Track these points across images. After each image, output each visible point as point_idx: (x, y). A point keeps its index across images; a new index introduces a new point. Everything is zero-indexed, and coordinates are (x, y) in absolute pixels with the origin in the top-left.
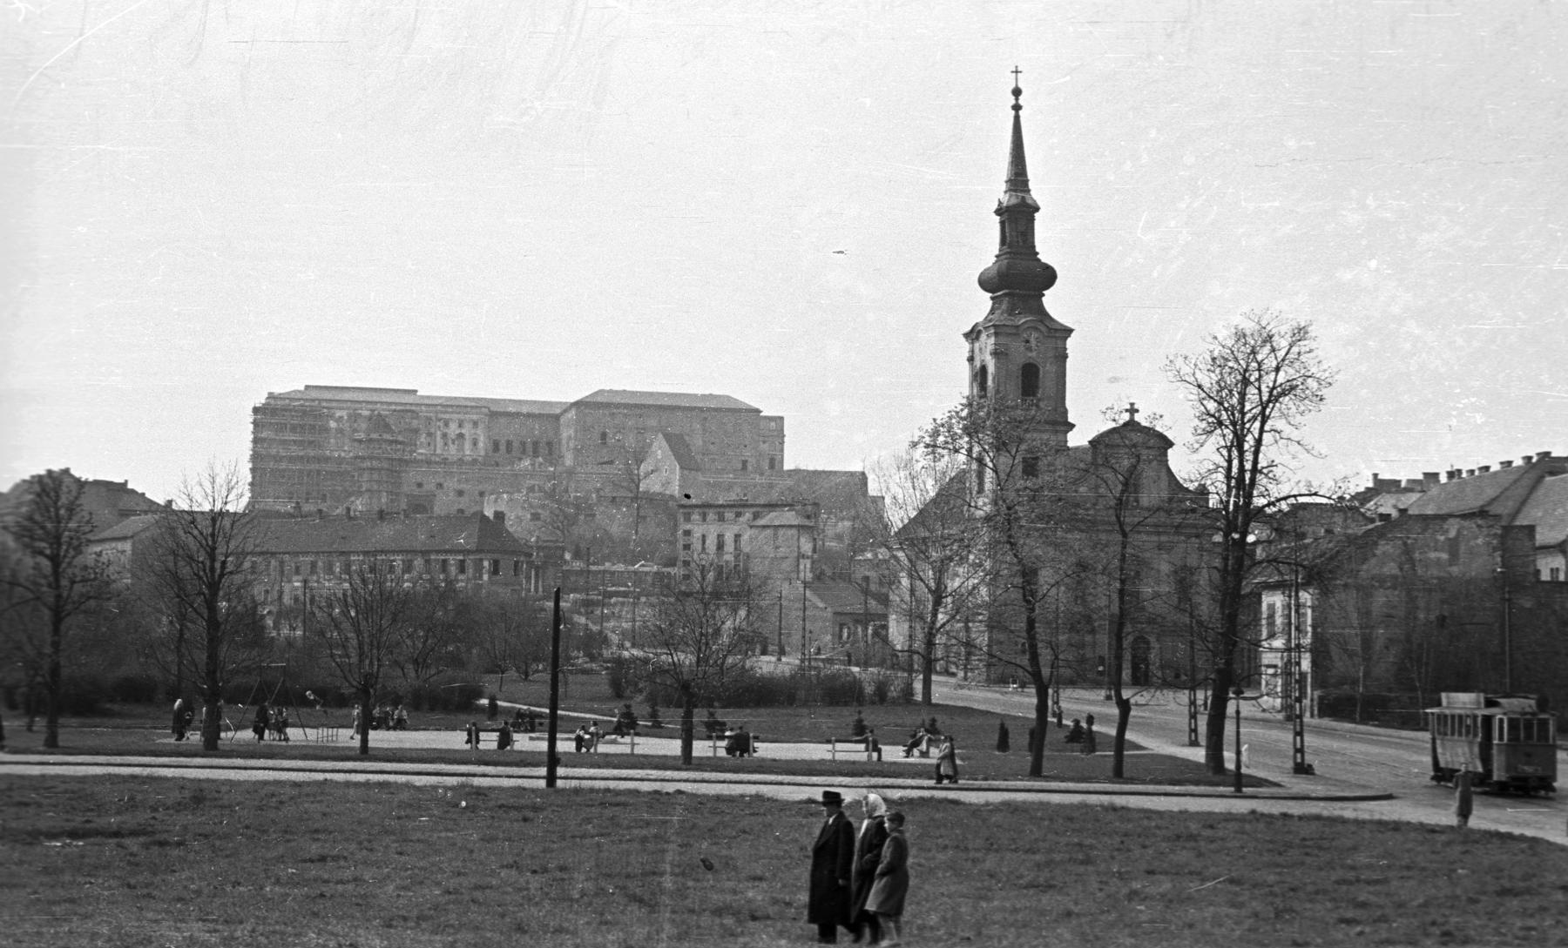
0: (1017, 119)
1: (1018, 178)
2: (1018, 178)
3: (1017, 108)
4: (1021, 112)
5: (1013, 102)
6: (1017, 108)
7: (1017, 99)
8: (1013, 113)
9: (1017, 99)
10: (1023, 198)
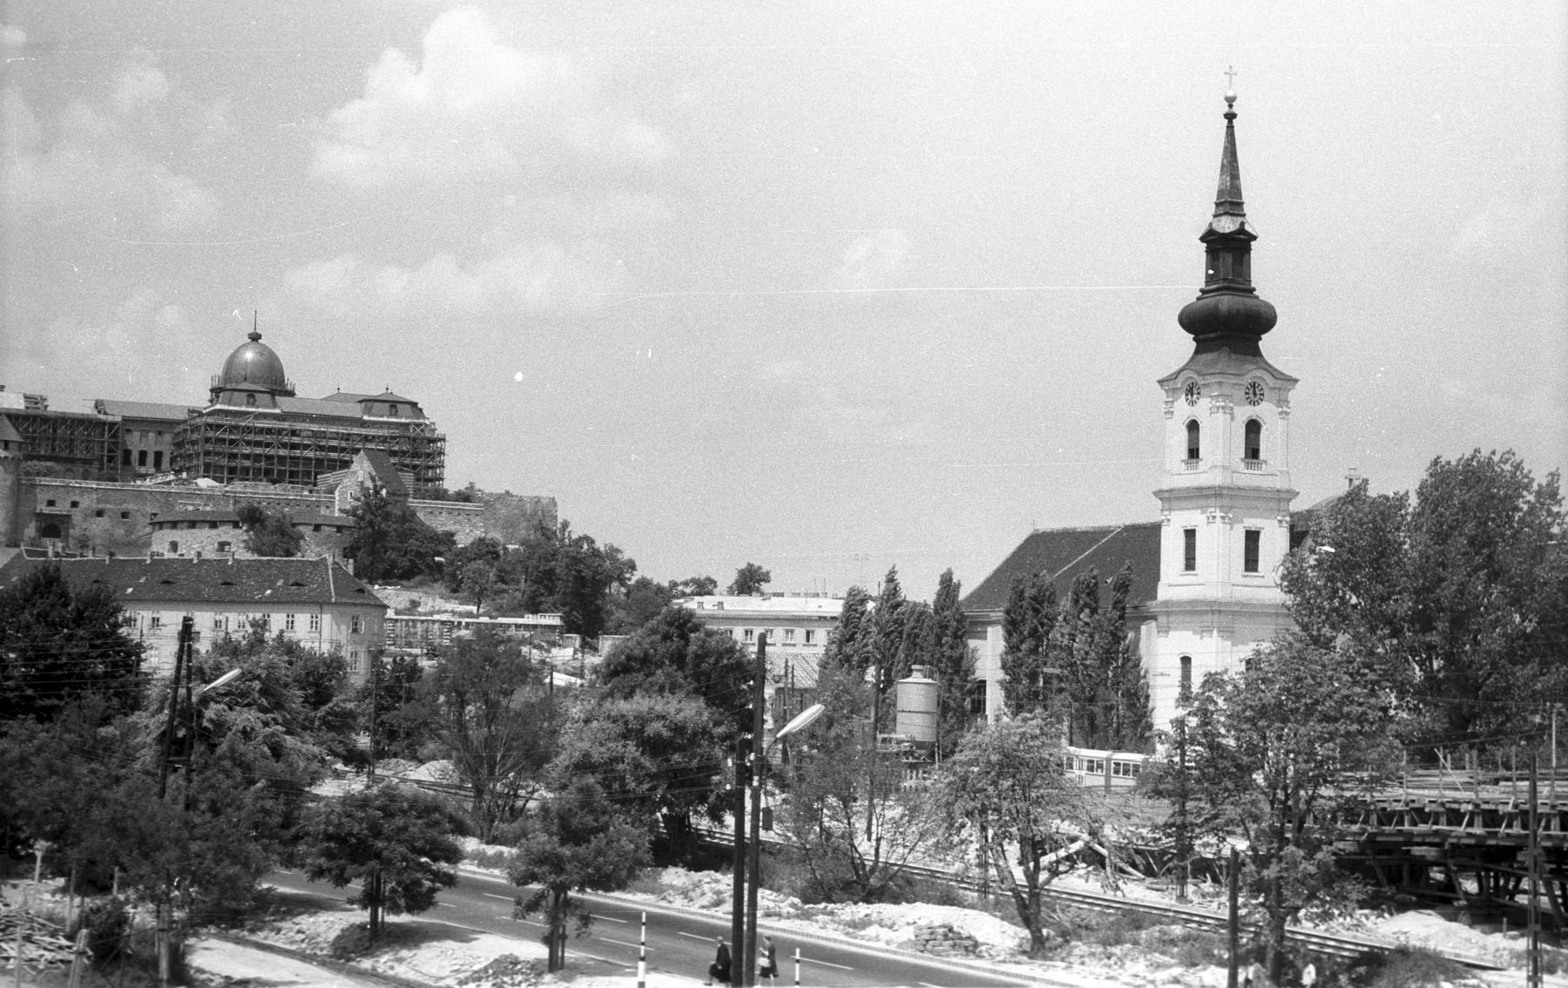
0: (1230, 128)
1: (1230, 202)
2: (1230, 202)
3: (1230, 117)
4: (1235, 121)
5: (1226, 109)
6: (1230, 117)
7: (1231, 106)
9: (1231, 106)
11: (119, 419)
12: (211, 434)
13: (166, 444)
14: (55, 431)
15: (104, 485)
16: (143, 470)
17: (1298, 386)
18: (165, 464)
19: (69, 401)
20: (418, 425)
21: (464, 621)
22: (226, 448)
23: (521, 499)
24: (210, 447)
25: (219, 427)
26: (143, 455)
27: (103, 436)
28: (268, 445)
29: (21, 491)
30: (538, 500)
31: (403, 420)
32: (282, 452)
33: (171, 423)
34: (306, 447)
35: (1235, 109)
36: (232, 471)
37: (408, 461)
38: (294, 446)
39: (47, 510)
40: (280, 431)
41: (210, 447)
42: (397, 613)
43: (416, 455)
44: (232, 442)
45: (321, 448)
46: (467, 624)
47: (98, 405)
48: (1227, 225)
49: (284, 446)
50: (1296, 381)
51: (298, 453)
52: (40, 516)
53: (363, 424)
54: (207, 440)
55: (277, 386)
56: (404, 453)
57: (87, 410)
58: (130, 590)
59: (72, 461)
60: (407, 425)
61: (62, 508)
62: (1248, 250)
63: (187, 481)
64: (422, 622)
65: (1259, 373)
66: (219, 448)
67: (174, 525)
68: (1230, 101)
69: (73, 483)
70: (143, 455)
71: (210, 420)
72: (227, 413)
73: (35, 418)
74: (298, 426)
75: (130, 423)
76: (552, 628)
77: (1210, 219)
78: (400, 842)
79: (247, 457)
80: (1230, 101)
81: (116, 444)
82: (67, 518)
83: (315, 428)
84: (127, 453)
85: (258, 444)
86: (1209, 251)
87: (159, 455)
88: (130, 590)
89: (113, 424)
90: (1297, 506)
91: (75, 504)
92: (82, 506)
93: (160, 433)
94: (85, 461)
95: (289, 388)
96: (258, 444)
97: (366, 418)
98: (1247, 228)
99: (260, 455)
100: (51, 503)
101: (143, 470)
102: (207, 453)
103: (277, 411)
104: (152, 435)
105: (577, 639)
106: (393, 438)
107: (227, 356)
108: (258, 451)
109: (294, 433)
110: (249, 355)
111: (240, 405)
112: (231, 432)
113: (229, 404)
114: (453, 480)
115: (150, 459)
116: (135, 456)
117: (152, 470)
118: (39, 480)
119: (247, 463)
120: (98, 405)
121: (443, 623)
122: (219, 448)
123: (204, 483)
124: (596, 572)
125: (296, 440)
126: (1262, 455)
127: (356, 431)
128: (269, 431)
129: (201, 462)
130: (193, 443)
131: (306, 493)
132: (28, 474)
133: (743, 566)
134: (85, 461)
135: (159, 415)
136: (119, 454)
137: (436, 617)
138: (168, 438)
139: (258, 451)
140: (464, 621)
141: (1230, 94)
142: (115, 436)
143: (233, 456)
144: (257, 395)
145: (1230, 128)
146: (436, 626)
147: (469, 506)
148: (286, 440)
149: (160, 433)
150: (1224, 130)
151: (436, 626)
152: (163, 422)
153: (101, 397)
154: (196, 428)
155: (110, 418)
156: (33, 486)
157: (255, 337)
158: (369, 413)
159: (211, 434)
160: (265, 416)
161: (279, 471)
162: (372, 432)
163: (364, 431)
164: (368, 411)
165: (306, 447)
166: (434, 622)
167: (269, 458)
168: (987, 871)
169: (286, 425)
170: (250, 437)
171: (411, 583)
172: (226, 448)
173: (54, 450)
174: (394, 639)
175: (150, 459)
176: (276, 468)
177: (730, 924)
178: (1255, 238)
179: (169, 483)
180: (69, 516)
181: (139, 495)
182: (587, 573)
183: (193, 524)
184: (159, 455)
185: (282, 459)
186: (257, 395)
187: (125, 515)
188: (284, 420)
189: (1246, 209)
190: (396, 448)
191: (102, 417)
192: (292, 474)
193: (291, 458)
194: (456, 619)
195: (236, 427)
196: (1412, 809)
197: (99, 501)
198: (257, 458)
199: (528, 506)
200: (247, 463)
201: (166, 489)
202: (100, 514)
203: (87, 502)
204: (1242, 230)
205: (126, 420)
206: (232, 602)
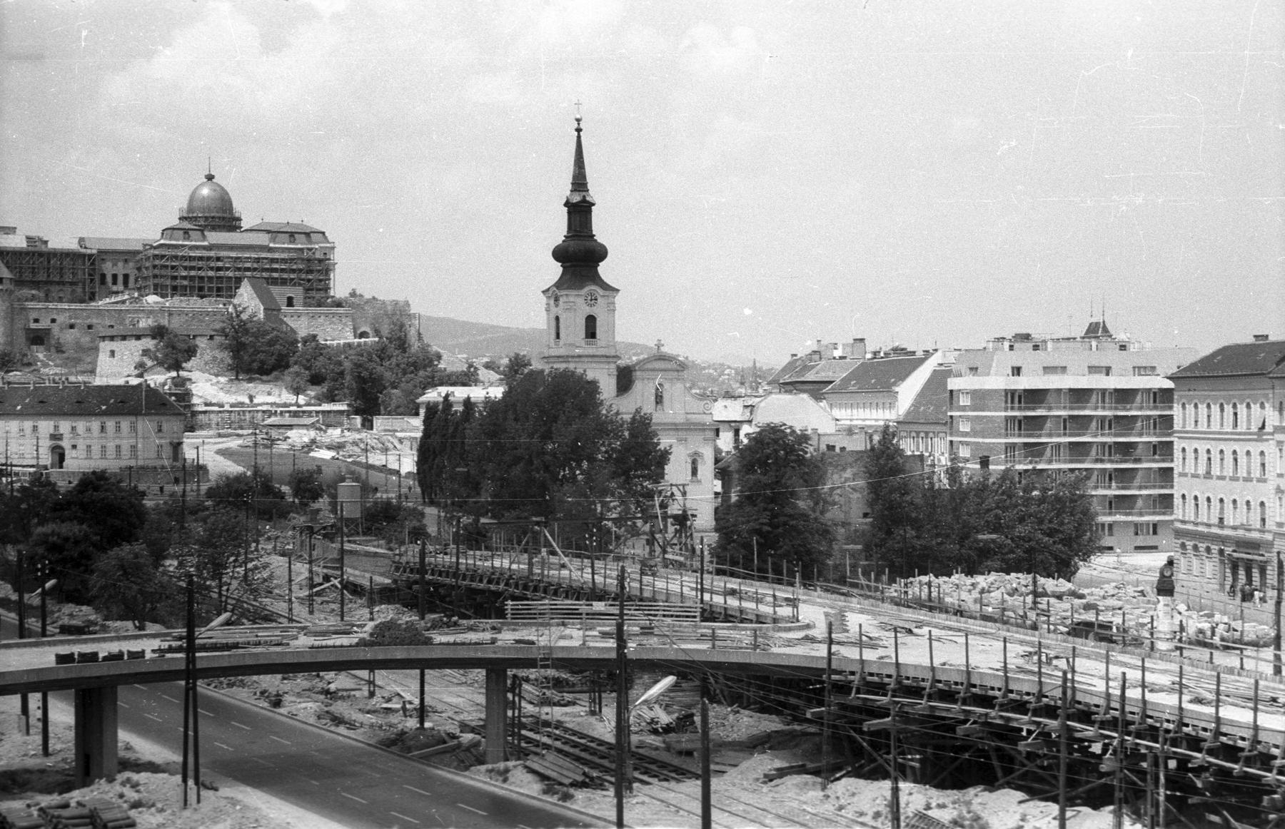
0: (579, 137)
2: (579, 182)
3: (579, 130)
4: (581, 133)
5: (576, 126)
6: (579, 130)
8: (576, 133)
10: (584, 197)
11: (94, 251)
12: (157, 262)
13: (130, 269)
14: (49, 262)
15: (73, 306)
16: (115, 288)
17: (620, 293)
18: (131, 284)
19: (62, 239)
20: (310, 249)
21: (279, 410)
22: (169, 272)
23: (384, 302)
24: (157, 272)
25: (163, 257)
26: (115, 277)
27: (84, 264)
28: (200, 269)
29: (15, 312)
30: (396, 303)
31: (299, 246)
32: (211, 273)
33: (136, 253)
34: (228, 269)
35: (581, 126)
36: (175, 288)
37: (303, 276)
38: (219, 269)
39: (33, 326)
40: (209, 258)
41: (157, 272)
42: (231, 406)
43: (310, 272)
44: (173, 267)
45: (239, 269)
46: (282, 412)
47: (81, 240)
48: (576, 198)
49: (212, 269)
50: (618, 291)
51: (221, 273)
52: (28, 330)
53: (270, 250)
54: (155, 267)
55: (224, 217)
56: (300, 270)
57: (73, 245)
58: (19, 408)
59: (63, 283)
60: (301, 250)
61: (44, 324)
62: (590, 212)
63: (136, 300)
64: (250, 411)
65: (593, 287)
66: (163, 272)
67: (112, 338)
68: (578, 120)
69: (51, 305)
70: (115, 277)
71: (157, 252)
72: (169, 246)
73: (34, 253)
74: (223, 254)
75: (104, 254)
76: (341, 412)
77: (568, 193)
78: (638, 504)
79: (184, 278)
80: (578, 120)
81: (94, 269)
82: (47, 332)
83: (233, 254)
84: (103, 276)
85: (192, 268)
86: (569, 213)
87: (126, 277)
88: (19, 408)
89: (90, 256)
90: (621, 363)
91: (53, 321)
92: (58, 321)
93: (126, 261)
94: (72, 284)
95: (237, 215)
96: (192, 268)
97: (271, 245)
98: (588, 199)
99: (194, 277)
100: (36, 321)
101: (115, 288)
102: (155, 276)
103: (206, 243)
104: (120, 264)
105: (358, 420)
106: (292, 260)
107: (192, 189)
108: (193, 273)
109: (218, 259)
110: (205, 191)
111: (178, 240)
112: (172, 261)
113: (170, 239)
114: (340, 287)
115: (120, 279)
116: (109, 279)
117: (121, 288)
118: (31, 305)
119: (185, 283)
120: (81, 240)
121: (264, 412)
122: (163, 272)
123: (152, 299)
124: (371, 374)
125: (220, 264)
126: (598, 337)
127: (264, 255)
128: (201, 258)
129: (151, 283)
130: (147, 268)
131: (221, 306)
132: (19, 300)
133: (512, 355)
134: (72, 284)
135: (121, 247)
136: (97, 278)
137: (259, 408)
138: (131, 264)
139: (193, 273)
140: (279, 410)
141: (578, 117)
142: (92, 264)
143: (175, 278)
144: (190, 232)
145: (579, 137)
146: (260, 414)
147: (341, 310)
148: (212, 264)
149: (126, 261)
150: (575, 139)
151: (260, 414)
152: (129, 252)
153: (85, 235)
154: (148, 259)
155: (89, 251)
156: (24, 309)
157: (210, 178)
158: (274, 242)
159: (157, 262)
160: (197, 247)
161: (209, 288)
162: (276, 256)
163: (269, 255)
164: (273, 240)
165: (228, 269)
166: (258, 411)
167: (201, 278)
168: (31, 607)
169: (212, 254)
170: (186, 264)
171: (269, 378)
172: (169, 272)
173: (49, 276)
174: (230, 424)
175: (120, 279)
176: (206, 285)
177: (17, 622)
178: (594, 205)
179: (123, 302)
180: (49, 330)
181: (99, 312)
182: (365, 374)
183: (124, 338)
184: (126, 277)
185: (210, 278)
186: (190, 232)
187: (90, 327)
188: (211, 250)
189: (589, 186)
190: (294, 267)
191: (83, 251)
192: (219, 289)
193: (217, 278)
194: (273, 409)
195: (176, 257)
196: (491, 551)
197: (70, 318)
198: (192, 278)
199: (389, 308)
200: (185, 283)
201: (119, 307)
202: (72, 327)
203: (61, 319)
204: (584, 200)
205: (101, 252)
206: (81, 415)
